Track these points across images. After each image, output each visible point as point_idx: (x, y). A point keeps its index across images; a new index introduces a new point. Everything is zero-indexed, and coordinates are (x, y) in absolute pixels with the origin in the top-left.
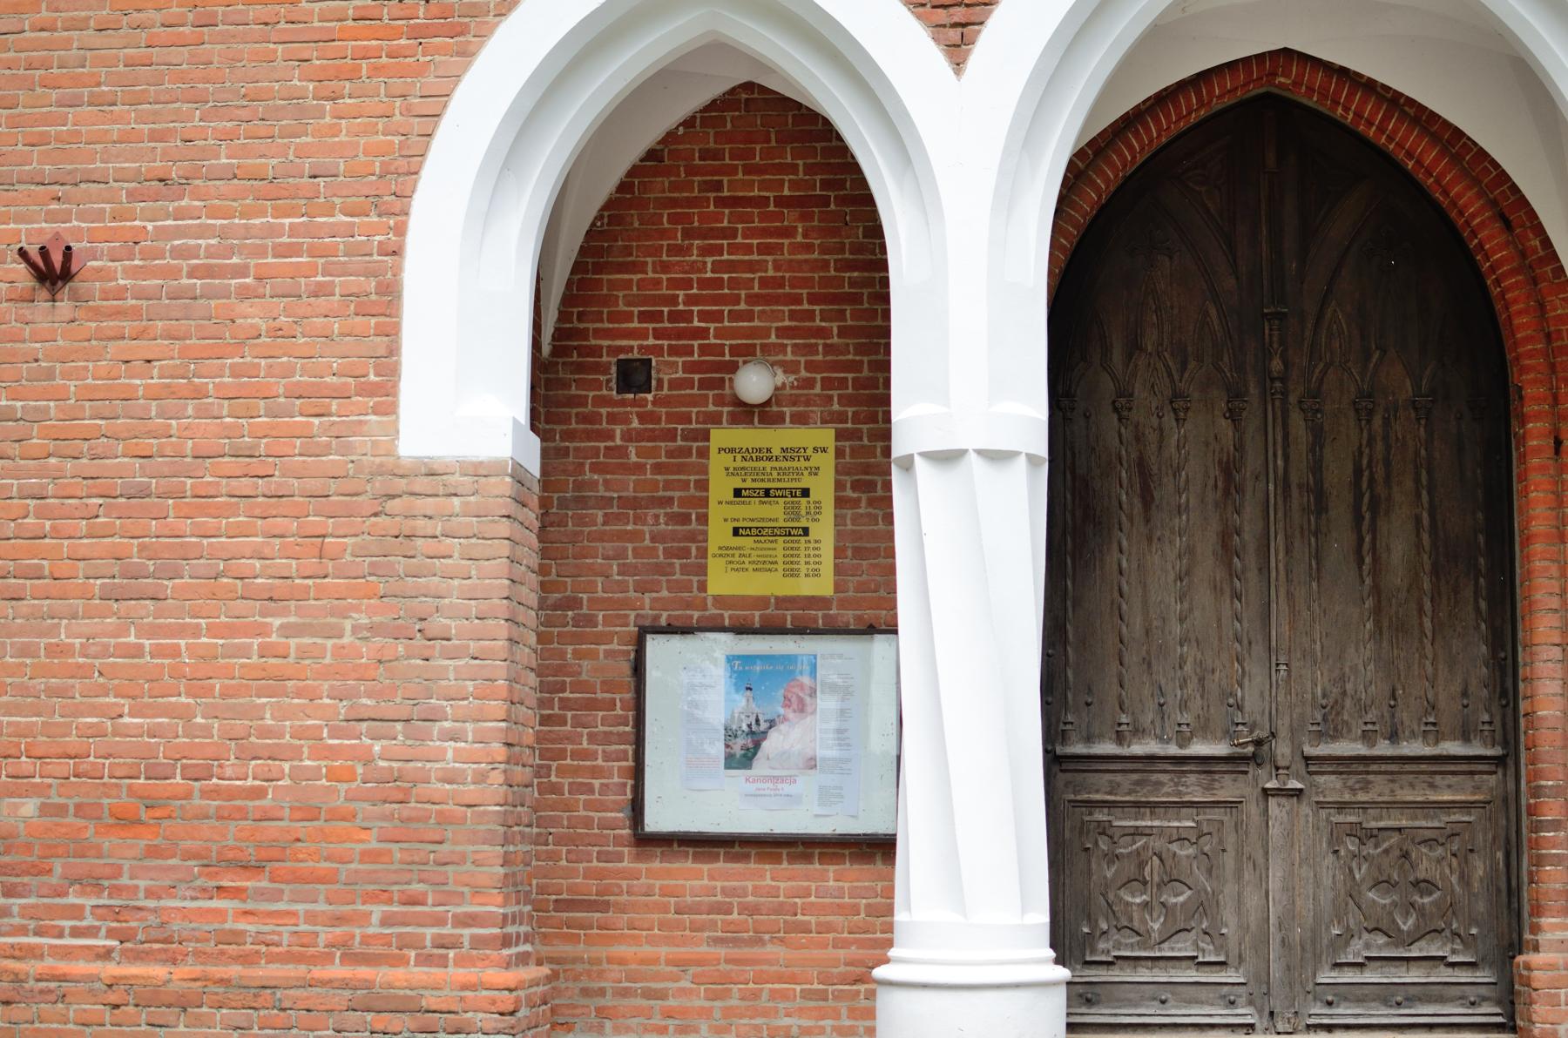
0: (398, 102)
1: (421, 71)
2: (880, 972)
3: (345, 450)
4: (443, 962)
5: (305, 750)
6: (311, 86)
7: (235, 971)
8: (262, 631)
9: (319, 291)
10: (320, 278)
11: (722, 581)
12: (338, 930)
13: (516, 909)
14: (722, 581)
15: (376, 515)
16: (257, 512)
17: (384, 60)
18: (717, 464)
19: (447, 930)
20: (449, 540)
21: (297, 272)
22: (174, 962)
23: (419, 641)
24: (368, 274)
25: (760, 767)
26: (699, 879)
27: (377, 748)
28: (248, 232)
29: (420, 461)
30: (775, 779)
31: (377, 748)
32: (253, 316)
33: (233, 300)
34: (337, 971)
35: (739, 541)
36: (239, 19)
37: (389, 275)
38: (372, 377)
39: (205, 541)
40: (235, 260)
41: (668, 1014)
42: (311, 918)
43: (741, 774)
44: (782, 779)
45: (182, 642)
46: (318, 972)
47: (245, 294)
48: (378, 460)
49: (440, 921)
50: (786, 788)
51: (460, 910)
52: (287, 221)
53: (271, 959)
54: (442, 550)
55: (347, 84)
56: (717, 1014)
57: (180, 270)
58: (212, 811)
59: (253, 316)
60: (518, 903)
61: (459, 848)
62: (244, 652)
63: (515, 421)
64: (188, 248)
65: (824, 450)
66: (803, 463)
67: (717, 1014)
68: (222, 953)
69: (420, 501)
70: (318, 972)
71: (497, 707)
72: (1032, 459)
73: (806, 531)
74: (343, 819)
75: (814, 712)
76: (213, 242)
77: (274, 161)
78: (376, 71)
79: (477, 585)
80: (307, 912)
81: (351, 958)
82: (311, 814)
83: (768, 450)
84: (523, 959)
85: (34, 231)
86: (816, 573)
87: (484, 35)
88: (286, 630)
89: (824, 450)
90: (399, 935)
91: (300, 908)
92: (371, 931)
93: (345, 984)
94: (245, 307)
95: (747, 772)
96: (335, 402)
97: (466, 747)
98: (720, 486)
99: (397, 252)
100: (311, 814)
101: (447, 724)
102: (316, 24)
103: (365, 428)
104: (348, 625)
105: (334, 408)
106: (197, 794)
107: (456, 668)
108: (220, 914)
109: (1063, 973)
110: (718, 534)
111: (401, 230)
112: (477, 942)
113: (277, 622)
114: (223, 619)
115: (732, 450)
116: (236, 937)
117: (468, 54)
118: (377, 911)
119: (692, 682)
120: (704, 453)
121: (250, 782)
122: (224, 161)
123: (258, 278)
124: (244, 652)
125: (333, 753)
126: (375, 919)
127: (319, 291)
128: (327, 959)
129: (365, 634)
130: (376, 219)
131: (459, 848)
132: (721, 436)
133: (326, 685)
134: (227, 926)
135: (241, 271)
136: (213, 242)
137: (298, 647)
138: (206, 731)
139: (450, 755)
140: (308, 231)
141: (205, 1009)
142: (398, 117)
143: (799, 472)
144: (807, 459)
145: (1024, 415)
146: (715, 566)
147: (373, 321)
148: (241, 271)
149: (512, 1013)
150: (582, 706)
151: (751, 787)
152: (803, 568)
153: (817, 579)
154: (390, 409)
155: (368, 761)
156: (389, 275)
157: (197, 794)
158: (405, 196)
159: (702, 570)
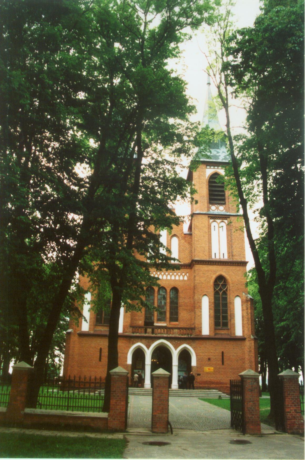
79: (130, 369)
153: (141, 368)
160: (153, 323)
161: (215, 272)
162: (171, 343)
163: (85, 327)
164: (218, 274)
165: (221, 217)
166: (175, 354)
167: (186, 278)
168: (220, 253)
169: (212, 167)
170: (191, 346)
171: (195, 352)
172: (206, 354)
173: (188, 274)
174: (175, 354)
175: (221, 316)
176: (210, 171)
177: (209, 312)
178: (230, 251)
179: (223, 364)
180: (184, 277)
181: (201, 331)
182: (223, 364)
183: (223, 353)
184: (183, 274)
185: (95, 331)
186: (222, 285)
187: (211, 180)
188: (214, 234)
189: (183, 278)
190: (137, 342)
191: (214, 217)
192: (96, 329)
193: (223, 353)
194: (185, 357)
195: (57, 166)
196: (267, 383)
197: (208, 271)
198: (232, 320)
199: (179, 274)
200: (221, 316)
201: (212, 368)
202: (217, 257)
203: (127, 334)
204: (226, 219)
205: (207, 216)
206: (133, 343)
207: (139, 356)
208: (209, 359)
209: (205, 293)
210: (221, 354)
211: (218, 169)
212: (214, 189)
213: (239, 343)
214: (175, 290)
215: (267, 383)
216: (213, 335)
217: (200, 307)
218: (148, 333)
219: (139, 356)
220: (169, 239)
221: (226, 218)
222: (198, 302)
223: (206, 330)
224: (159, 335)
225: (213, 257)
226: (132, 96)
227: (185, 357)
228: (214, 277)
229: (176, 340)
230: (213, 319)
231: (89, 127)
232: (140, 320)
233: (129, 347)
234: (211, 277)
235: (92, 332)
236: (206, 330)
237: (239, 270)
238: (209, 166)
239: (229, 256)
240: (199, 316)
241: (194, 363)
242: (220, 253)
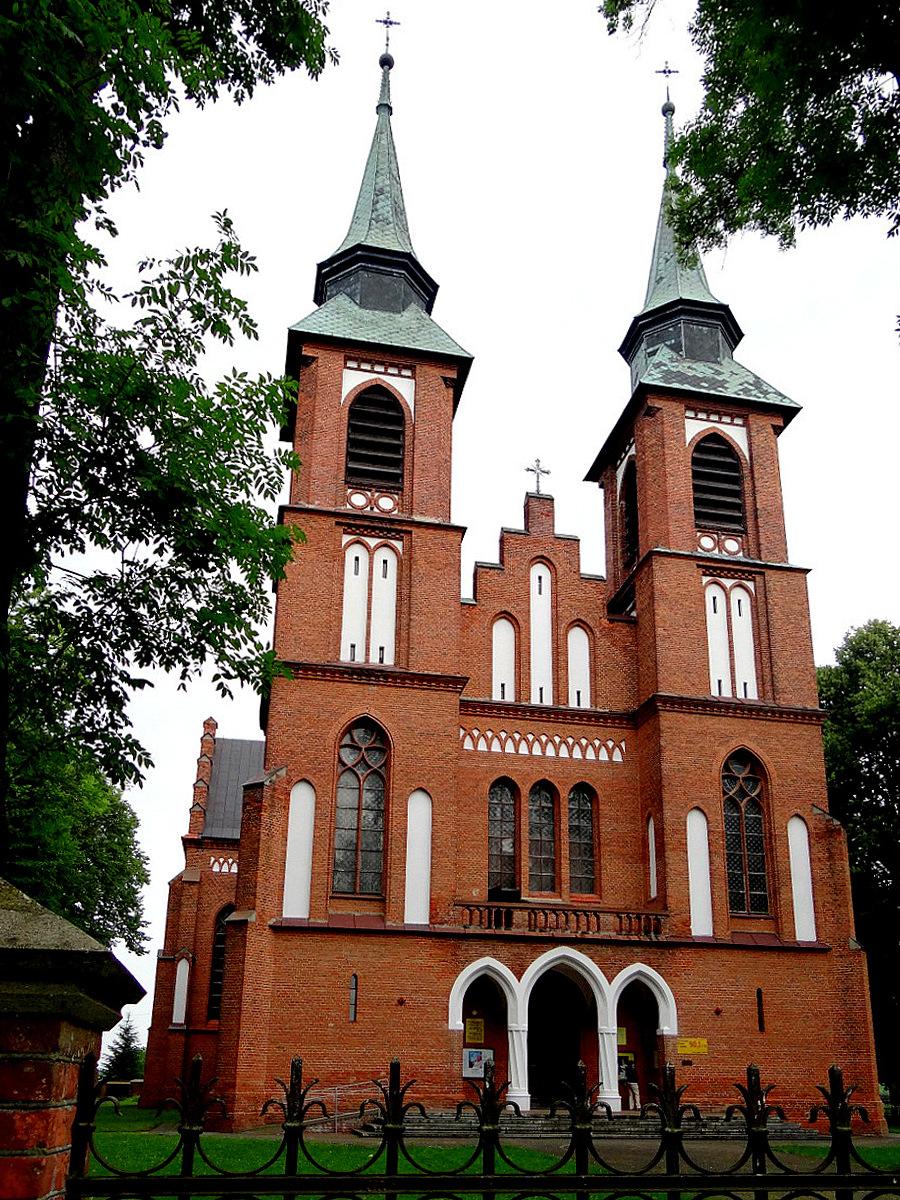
85: (398, 997)
145: (525, 1026)
160: (519, 894)
161: (724, 739)
163: (296, 904)
164: (734, 745)
165: (374, 529)
166: (608, 995)
167: (617, 757)
168: (733, 681)
169: (702, 416)
171: (672, 989)
172: (707, 996)
173: (623, 745)
174: (608, 995)
175: (750, 878)
176: (695, 427)
177: (711, 863)
178: (768, 678)
179: (762, 1029)
180: (610, 753)
181: (687, 923)
182: (762, 1029)
183: (759, 992)
184: (221, 860)
185: (331, 917)
186: (744, 779)
187: (358, 408)
188: (715, 623)
189: (230, 869)
190: (481, 956)
191: (716, 568)
192: (331, 911)
193: (759, 992)
194: (638, 1005)
195: (52, 634)
196: (179, 1016)
197: (703, 733)
198: (783, 890)
199: (221, 860)
200: (750, 878)
201: (704, 1042)
202: (727, 693)
203: (445, 928)
204: (754, 580)
205: (694, 563)
207: (486, 999)
208: (718, 1012)
209: (695, 803)
210: (755, 997)
211: (719, 422)
212: (705, 483)
213: (809, 961)
214: (583, 789)
215: (179, 1016)
216: (725, 937)
217: (683, 847)
218: (518, 927)
219: (486, 999)
220: (562, 632)
221: (750, 573)
222: (675, 832)
223: (701, 924)
224: (558, 933)
225: (715, 692)
226: (127, 608)
227: (638, 1005)
228: (724, 753)
229: (612, 951)
230: (722, 885)
231: (47, 663)
232: (474, 885)
234: (715, 754)
235: (322, 922)
236: (701, 924)
237: (800, 737)
238: (381, 363)
239: (762, 692)
240: (680, 874)
241: (668, 1024)
242: (733, 681)
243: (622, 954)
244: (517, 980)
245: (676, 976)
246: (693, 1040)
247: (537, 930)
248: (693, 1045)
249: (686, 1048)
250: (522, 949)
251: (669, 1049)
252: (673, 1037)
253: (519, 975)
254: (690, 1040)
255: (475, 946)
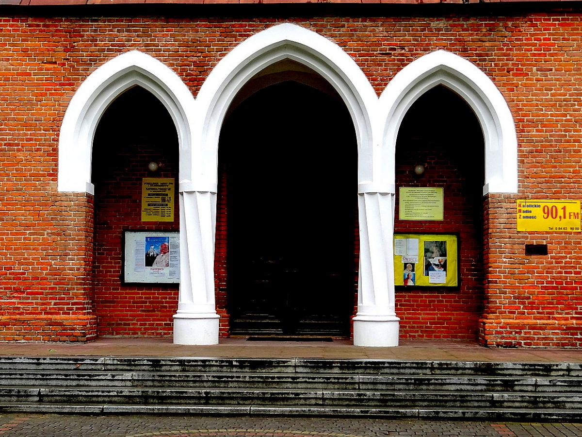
0: (57, 102)
1: (62, 94)
2: (174, 316)
3: (45, 190)
4: (69, 314)
5: (35, 263)
6: (34, 97)
7: (18, 316)
8: (24, 234)
9: (38, 150)
10: (38, 147)
11: (145, 218)
12: (43, 306)
13: (87, 301)
14: (145, 218)
15: (53, 206)
16: (23, 205)
17: (53, 91)
18: (144, 187)
19: (70, 306)
20: (70, 212)
21: (32, 145)
22: (3, 315)
23: (63, 237)
24: (50, 146)
25: (154, 266)
26: (140, 294)
27: (53, 262)
28: (19, 135)
29: (63, 193)
30: (159, 269)
31: (53, 262)
32: (21, 156)
33: (16, 152)
34: (43, 316)
35: (149, 207)
36: (15, 79)
37: (55, 147)
38: (51, 172)
39: (10, 212)
40: (16, 142)
41: (130, 329)
42: (37, 303)
43: (149, 268)
44: (159, 269)
45: (4, 237)
46: (38, 316)
47: (19, 150)
48: (53, 192)
49: (68, 304)
50: (161, 271)
51: (73, 301)
52: (29, 132)
53: (27, 314)
54: (69, 214)
55: (44, 97)
56: (143, 329)
57: (2, 144)
58: (572, 171)
59: (21, 156)
60: (88, 300)
61: (73, 287)
62: (20, 239)
63: (87, 183)
64: (4, 138)
65: (172, 184)
66: (167, 187)
67: (143, 329)
68: (15, 312)
69: (63, 203)
70: (38, 316)
71: (82, 252)
72: (213, 193)
73: (167, 205)
74: (45, 280)
75: (168, 252)
76: (11, 137)
77: (26, 117)
78: (51, 94)
79: (76, 222)
80: (35, 302)
81: (46, 313)
82: (37, 278)
83: (158, 183)
84: (88, 313)
86: (169, 216)
87: (79, 85)
88: (30, 234)
89: (172, 184)
90: (58, 307)
91: (34, 301)
92: (51, 307)
93: (45, 319)
94: (19, 153)
95: (152, 267)
96: (42, 178)
97: (74, 264)
98: (145, 193)
99: (57, 140)
100: (37, 278)
101: (70, 257)
102: (35, 82)
103: (49, 184)
104: (46, 232)
105: (42, 179)
106: (8, 274)
107: (72, 243)
108: (14, 303)
109: (218, 316)
110: (144, 205)
111: (58, 135)
112: (77, 309)
113: (28, 232)
114: (15, 231)
115: (148, 184)
116: (18, 308)
117: (74, 90)
118: (53, 302)
119: (135, 244)
120: (141, 184)
121: (21, 271)
122: (12, 116)
123: (22, 146)
124: (20, 239)
125: (42, 264)
126: (52, 304)
127: (38, 150)
128: (41, 313)
129: (50, 235)
130: (52, 132)
131: (73, 287)
132: (145, 180)
133: (40, 247)
134: (16, 306)
135: (18, 145)
136: (11, 137)
137: (33, 238)
138: (10, 259)
139: (71, 264)
140: (34, 135)
141: (10, 326)
142: (57, 107)
143: (165, 189)
144: (168, 186)
146: (143, 214)
147: (51, 158)
148: (18, 145)
149: (85, 326)
150: (104, 247)
151: (152, 271)
152: (166, 214)
154: (56, 180)
155: (51, 265)
156: (55, 147)
157: (8, 274)
158: (59, 126)
159: (140, 215)
162: (342, 44)
166: (377, 121)
170: (479, 60)
171: (510, 102)
190: (120, 49)
194: (440, 139)
206: (96, 60)
207: (136, 135)
219: (136, 135)
227: (440, 139)
233: (72, 84)
243: (404, 33)
244: (189, 94)
245: (520, 73)
246: (550, 204)
247: (564, 262)
248: (550, 213)
249: (534, 221)
250: (201, 32)
251: (498, 220)
252: (509, 198)
253: (194, 83)
254: (543, 203)
255: (110, 31)
